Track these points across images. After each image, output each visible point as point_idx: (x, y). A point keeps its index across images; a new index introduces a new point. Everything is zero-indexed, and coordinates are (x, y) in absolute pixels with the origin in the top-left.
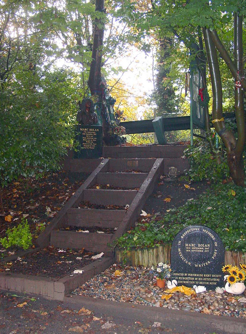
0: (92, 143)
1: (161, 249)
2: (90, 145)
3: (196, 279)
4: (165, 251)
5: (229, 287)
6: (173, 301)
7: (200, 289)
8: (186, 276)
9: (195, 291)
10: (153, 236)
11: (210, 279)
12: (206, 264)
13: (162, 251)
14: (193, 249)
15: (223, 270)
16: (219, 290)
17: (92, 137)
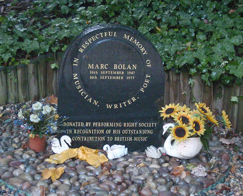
1: (32, 68)
3: (109, 132)
4: (39, 72)
5: (172, 147)
6: (67, 182)
7: (117, 151)
9: (106, 155)
10: (14, 43)
11: (136, 132)
12: (127, 104)
13: (34, 73)
14: (102, 75)
15: (162, 115)
16: (152, 152)
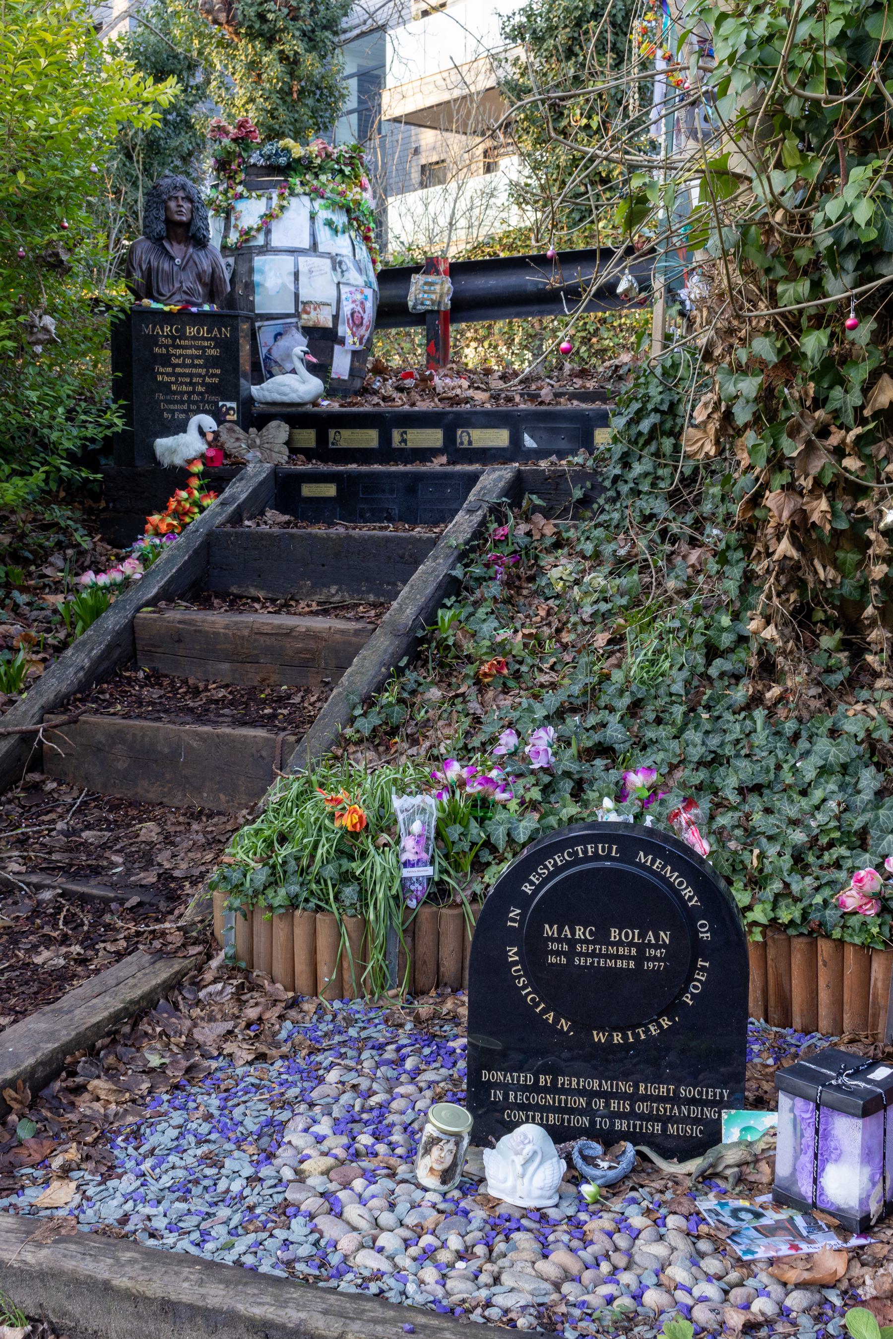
0: (201, 393)
2: (190, 402)
8: (545, 1090)
11: (672, 1109)
17: (200, 366)
